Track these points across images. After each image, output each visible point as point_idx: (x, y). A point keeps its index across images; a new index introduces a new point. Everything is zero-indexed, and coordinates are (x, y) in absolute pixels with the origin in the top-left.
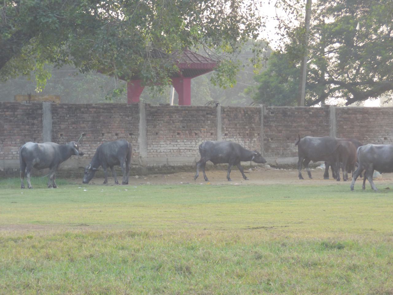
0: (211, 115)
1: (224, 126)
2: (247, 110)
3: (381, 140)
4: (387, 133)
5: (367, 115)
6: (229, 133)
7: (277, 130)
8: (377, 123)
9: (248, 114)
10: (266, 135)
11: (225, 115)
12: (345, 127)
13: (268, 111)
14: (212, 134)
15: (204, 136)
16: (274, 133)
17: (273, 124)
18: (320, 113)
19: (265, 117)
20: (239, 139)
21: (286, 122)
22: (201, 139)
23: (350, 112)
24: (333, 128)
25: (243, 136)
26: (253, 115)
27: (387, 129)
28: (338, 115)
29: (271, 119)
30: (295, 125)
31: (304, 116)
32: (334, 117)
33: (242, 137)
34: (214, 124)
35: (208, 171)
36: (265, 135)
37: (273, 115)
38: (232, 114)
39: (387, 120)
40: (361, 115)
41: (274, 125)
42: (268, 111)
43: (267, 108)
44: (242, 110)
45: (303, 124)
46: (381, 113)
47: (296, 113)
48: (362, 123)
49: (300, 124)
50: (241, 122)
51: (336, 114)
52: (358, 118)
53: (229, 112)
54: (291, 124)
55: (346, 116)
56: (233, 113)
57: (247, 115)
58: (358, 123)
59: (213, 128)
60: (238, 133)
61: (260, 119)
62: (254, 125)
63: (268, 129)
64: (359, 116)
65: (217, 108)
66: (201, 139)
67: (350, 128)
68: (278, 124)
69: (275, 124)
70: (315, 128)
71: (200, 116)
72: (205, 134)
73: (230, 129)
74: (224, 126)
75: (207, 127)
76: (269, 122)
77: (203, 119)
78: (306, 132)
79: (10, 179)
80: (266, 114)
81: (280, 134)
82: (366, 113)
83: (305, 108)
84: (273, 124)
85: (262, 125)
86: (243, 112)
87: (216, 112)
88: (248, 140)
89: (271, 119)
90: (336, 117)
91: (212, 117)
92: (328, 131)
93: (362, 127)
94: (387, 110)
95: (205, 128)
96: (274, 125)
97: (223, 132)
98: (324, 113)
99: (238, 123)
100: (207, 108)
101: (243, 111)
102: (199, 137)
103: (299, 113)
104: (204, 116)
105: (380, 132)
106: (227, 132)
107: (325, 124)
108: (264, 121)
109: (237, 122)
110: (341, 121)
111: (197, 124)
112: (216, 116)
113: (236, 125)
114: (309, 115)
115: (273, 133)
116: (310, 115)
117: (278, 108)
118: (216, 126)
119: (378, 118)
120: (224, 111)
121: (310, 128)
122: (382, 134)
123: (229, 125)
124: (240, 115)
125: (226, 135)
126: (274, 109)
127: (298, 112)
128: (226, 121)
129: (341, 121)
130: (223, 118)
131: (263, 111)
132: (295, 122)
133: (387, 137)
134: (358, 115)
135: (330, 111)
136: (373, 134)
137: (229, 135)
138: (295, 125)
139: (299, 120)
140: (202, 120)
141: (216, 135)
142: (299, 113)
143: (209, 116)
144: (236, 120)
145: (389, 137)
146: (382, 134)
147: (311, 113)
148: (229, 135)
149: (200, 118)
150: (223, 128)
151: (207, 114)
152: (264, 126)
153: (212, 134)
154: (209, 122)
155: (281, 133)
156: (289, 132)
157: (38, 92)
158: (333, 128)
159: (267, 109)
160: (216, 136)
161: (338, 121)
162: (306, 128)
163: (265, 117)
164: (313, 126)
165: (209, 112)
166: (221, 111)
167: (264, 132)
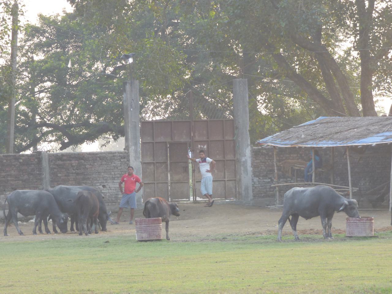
3: (99, 188)
4: (106, 180)
5: (83, 161)
8: (95, 170)
12: (59, 175)
18: (32, 160)
23: (65, 158)
24: (47, 176)
27: (105, 175)
28: (52, 161)
31: (13, 164)
32: (47, 164)
39: (105, 166)
40: (77, 162)
45: (13, 172)
46: (98, 159)
48: (77, 170)
49: (10, 173)
51: (49, 161)
52: (73, 165)
55: (60, 162)
58: (74, 170)
64: (75, 163)
67: (66, 176)
70: (26, 177)
82: (82, 159)
90: (49, 165)
92: (41, 180)
93: (78, 174)
94: (105, 155)
98: (36, 160)
103: (8, 161)
105: (98, 179)
107: (38, 172)
110: (55, 168)
112: (252, 164)
114: (19, 164)
116: (20, 163)
119: (95, 164)
121: (21, 178)
122: (100, 181)
127: (7, 160)
129: (55, 168)
132: (3, 171)
133: (105, 184)
134: (73, 162)
135: (42, 158)
136: (90, 182)
145: (108, 185)
146: (100, 181)
147: (21, 161)
158: (47, 176)
161: (51, 169)
164: (24, 175)
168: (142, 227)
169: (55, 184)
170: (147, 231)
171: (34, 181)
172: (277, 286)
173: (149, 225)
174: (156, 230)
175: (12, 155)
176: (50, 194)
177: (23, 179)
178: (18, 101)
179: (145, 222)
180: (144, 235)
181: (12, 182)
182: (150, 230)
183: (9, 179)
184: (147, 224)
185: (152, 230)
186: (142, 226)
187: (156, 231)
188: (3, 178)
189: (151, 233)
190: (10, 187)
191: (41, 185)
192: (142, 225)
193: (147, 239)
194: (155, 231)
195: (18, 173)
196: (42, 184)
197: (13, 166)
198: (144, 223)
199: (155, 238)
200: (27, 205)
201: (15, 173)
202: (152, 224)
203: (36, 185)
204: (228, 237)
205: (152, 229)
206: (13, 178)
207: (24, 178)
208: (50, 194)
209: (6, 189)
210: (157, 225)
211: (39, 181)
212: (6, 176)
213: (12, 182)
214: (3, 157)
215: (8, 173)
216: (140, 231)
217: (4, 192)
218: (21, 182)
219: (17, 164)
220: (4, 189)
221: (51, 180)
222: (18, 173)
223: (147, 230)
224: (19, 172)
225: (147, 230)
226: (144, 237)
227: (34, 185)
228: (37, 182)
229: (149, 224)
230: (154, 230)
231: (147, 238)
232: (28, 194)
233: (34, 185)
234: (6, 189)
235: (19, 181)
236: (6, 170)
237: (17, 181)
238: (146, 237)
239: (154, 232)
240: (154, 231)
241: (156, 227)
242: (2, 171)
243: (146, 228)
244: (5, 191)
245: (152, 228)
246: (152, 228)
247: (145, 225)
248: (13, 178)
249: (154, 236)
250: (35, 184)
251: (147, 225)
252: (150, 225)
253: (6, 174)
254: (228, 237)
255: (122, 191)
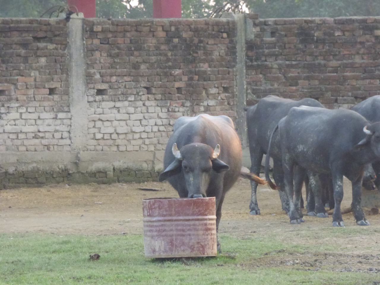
0: (51, 41)
1: (92, 71)
2: (177, 29)
6: (110, 87)
7: (285, 77)
9: (179, 37)
10: (254, 92)
11: (96, 42)
13: (258, 29)
14: (52, 91)
15: (25, 98)
16: (276, 86)
17: (273, 63)
19: (250, 46)
20: (147, 103)
21: (308, 58)
22: (14, 105)
25: (163, 94)
26: (201, 41)
29: (266, 51)
30: (334, 63)
31: (359, 40)
33: (159, 96)
34: (60, 66)
35: (38, 187)
36: (249, 91)
37: (273, 39)
38: (120, 40)
41: (275, 66)
42: (258, 29)
43: (257, 21)
44: (160, 29)
45: (358, 60)
47: (337, 34)
49: (350, 61)
50: (153, 58)
53: (110, 35)
54: (323, 62)
56: (124, 36)
57: (176, 40)
59: (56, 77)
60: (145, 88)
61: (232, 51)
62: (207, 65)
63: (261, 76)
65: (70, 24)
66: (17, 105)
68: (287, 62)
69: (280, 62)
71: (14, 46)
72: (31, 92)
73: (114, 79)
74: (92, 71)
75: (37, 73)
76: (263, 59)
77: (23, 52)
78: (368, 81)
79: (191, 173)
80: (253, 36)
81: (294, 88)
83: (364, 21)
84: (273, 63)
85: (240, 66)
86: (161, 34)
87: (67, 35)
88: (183, 105)
89: (266, 51)
91: (51, 46)
95: (30, 76)
96: (275, 66)
97: (92, 86)
99: (144, 62)
100: (35, 25)
101: (163, 30)
102: (10, 100)
103: (347, 34)
104: (25, 45)
106: (104, 86)
108: (247, 55)
109: (139, 59)
111: (4, 66)
112: (65, 45)
113: (136, 66)
114: (373, 40)
115: (272, 85)
117: (285, 23)
118: (66, 70)
120: (92, 31)
123: (112, 67)
124: (151, 42)
125: (100, 92)
126: (276, 23)
127: (343, 31)
128: (101, 57)
130: (89, 51)
131: (246, 31)
137: (110, 92)
138: (334, 63)
139: (346, 52)
140: (19, 55)
141: (67, 93)
142: (347, 34)
143: (41, 45)
144: (136, 53)
148: (110, 92)
149: (11, 51)
150: (89, 78)
151: (37, 39)
152: (248, 67)
153: (52, 91)
154: (43, 60)
155: (296, 84)
156: (317, 82)
157: (182, 12)
159: (255, 25)
160: (65, 97)
162: (365, 71)
163: (250, 46)
165: (41, 35)
166: (84, 31)
167: (249, 83)
168: (153, 221)
170: (164, 233)
173: (170, 218)
174: (189, 230)
175: (357, 20)
179: (160, 208)
180: (157, 242)
181: (354, 83)
182: (171, 230)
183: (348, 74)
184: (165, 213)
185: (177, 230)
186: (154, 219)
187: (190, 235)
188: (333, 73)
189: (174, 238)
190: (350, 94)
192: (155, 217)
193: (163, 256)
194: (188, 232)
195: (371, 61)
197: (359, 46)
198: (157, 212)
199: (187, 253)
200: (301, 148)
201: (363, 61)
202: (180, 216)
205: (179, 228)
210: (200, 217)
212: (340, 67)
213: (354, 83)
214: (335, 23)
215: (345, 61)
216: (148, 233)
217: (335, 104)
219: (368, 41)
220: (335, 98)
222: (371, 61)
223: (164, 230)
224: (374, 60)
225: (164, 230)
226: (157, 249)
229: (171, 215)
230: (183, 231)
231: (165, 251)
232: (309, 120)
235: (372, 81)
236: (342, 54)
238: (162, 249)
239: (183, 235)
240: (184, 233)
241: (192, 223)
242: (331, 57)
243: (162, 225)
244: (336, 101)
245: (177, 225)
246: (177, 225)
247: (160, 215)
249: (182, 248)
251: (165, 216)
252: (174, 218)
253: (340, 62)
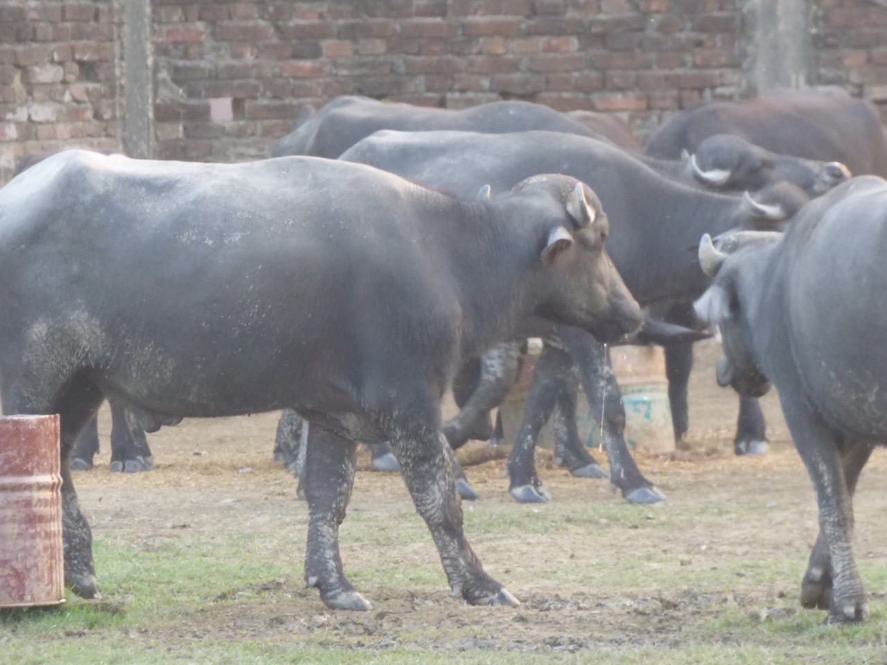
169: (847, 62)
171: (682, 36)
172: (181, 647)
176: (436, 194)
177: (593, 23)
178: (484, 438)
188: (432, 14)
190: (485, 83)
191: (735, 65)
196: (745, 65)
203: (695, 66)
204: (771, 550)
206: (510, 18)
207: (602, 17)
208: (436, 194)
209: (449, 95)
211: (718, 37)
218: (574, 43)
221: (814, 31)
227: (679, 71)
228: (699, 44)
233: (679, 71)
234: (449, 95)
237: (541, 41)
248: (510, 18)
250: (683, 64)
254: (771, 550)
255: (534, 480)
